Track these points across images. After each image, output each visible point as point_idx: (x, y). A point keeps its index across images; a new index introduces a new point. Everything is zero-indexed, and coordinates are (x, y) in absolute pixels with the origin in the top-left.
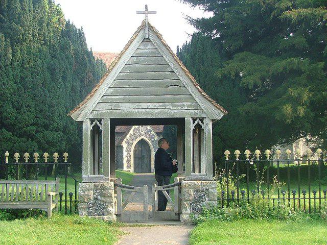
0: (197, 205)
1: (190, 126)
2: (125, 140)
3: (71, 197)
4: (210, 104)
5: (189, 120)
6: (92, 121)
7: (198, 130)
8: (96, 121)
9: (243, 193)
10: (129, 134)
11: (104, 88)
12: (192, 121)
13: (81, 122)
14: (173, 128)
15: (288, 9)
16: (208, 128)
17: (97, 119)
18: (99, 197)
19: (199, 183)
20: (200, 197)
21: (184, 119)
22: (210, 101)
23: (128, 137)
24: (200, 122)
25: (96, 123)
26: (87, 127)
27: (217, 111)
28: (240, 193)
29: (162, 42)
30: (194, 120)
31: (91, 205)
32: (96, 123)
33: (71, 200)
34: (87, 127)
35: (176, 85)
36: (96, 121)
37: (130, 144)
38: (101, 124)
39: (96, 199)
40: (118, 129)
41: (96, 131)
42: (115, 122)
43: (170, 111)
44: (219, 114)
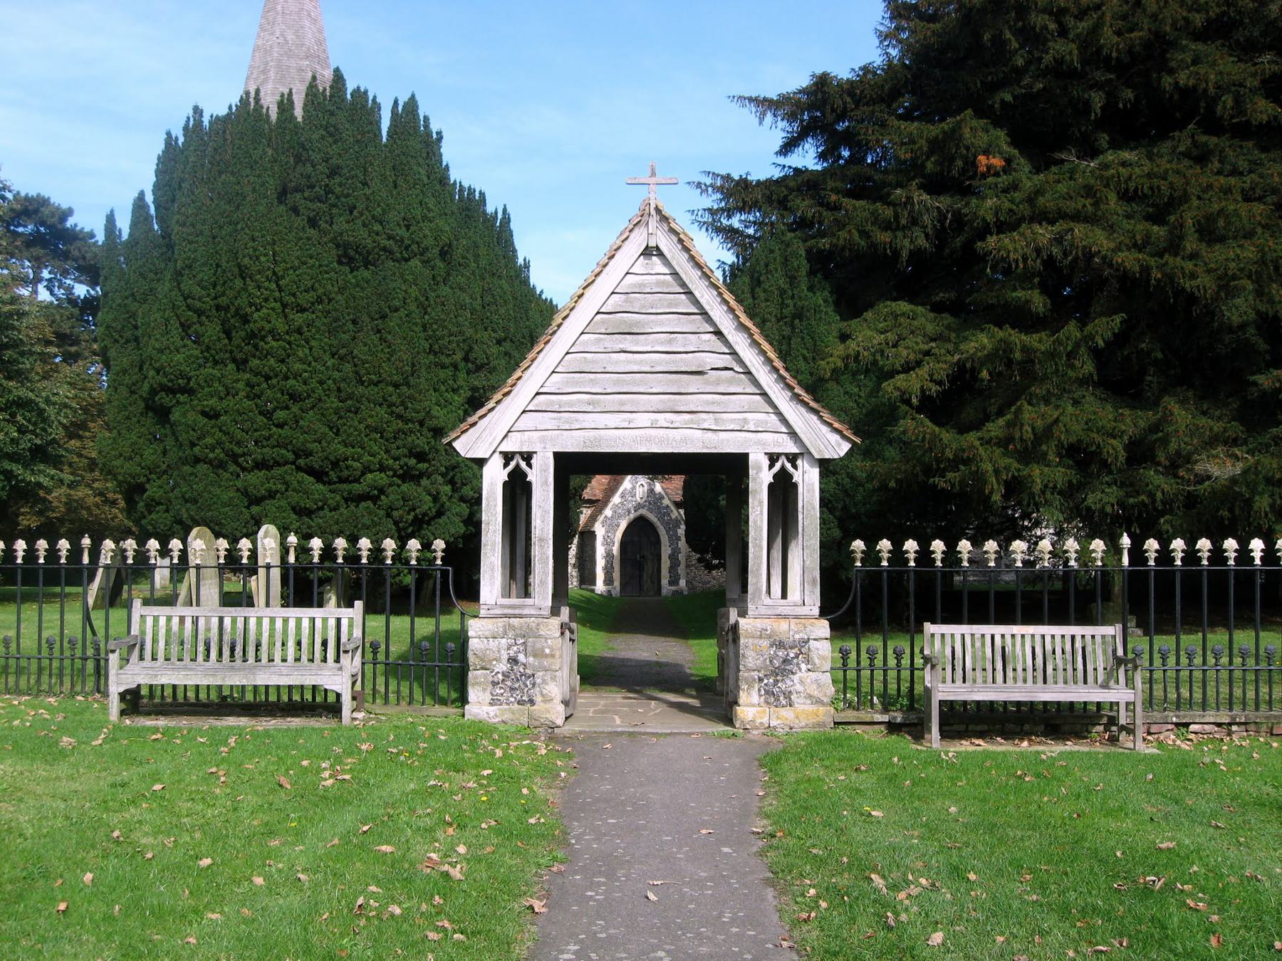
0: (776, 682)
1: (761, 479)
2: (601, 518)
3: (375, 653)
4: (815, 418)
5: (758, 460)
6: (508, 457)
7: (783, 490)
8: (518, 458)
9: (872, 654)
10: (610, 505)
11: (541, 371)
12: (766, 462)
13: (481, 462)
14: (713, 483)
15: (1003, 227)
16: (808, 480)
17: (521, 453)
18: (521, 657)
19: (783, 625)
20: (785, 661)
21: (745, 456)
22: (816, 412)
23: (608, 512)
24: (788, 466)
25: (518, 466)
26: (494, 478)
27: (835, 438)
28: (864, 655)
29: (692, 258)
30: (773, 458)
31: (500, 676)
32: (518, 466)
33: (375, 658)
34: (494, 478)
35: (726, 369)
36: (518, 458)
37: (612, 527)
38: (530, 465)
39: (513, 661)
40: (575, 481)
41: (517, 489)
42: (563, 460)
43: (710, 434)
44: (839, 445)
